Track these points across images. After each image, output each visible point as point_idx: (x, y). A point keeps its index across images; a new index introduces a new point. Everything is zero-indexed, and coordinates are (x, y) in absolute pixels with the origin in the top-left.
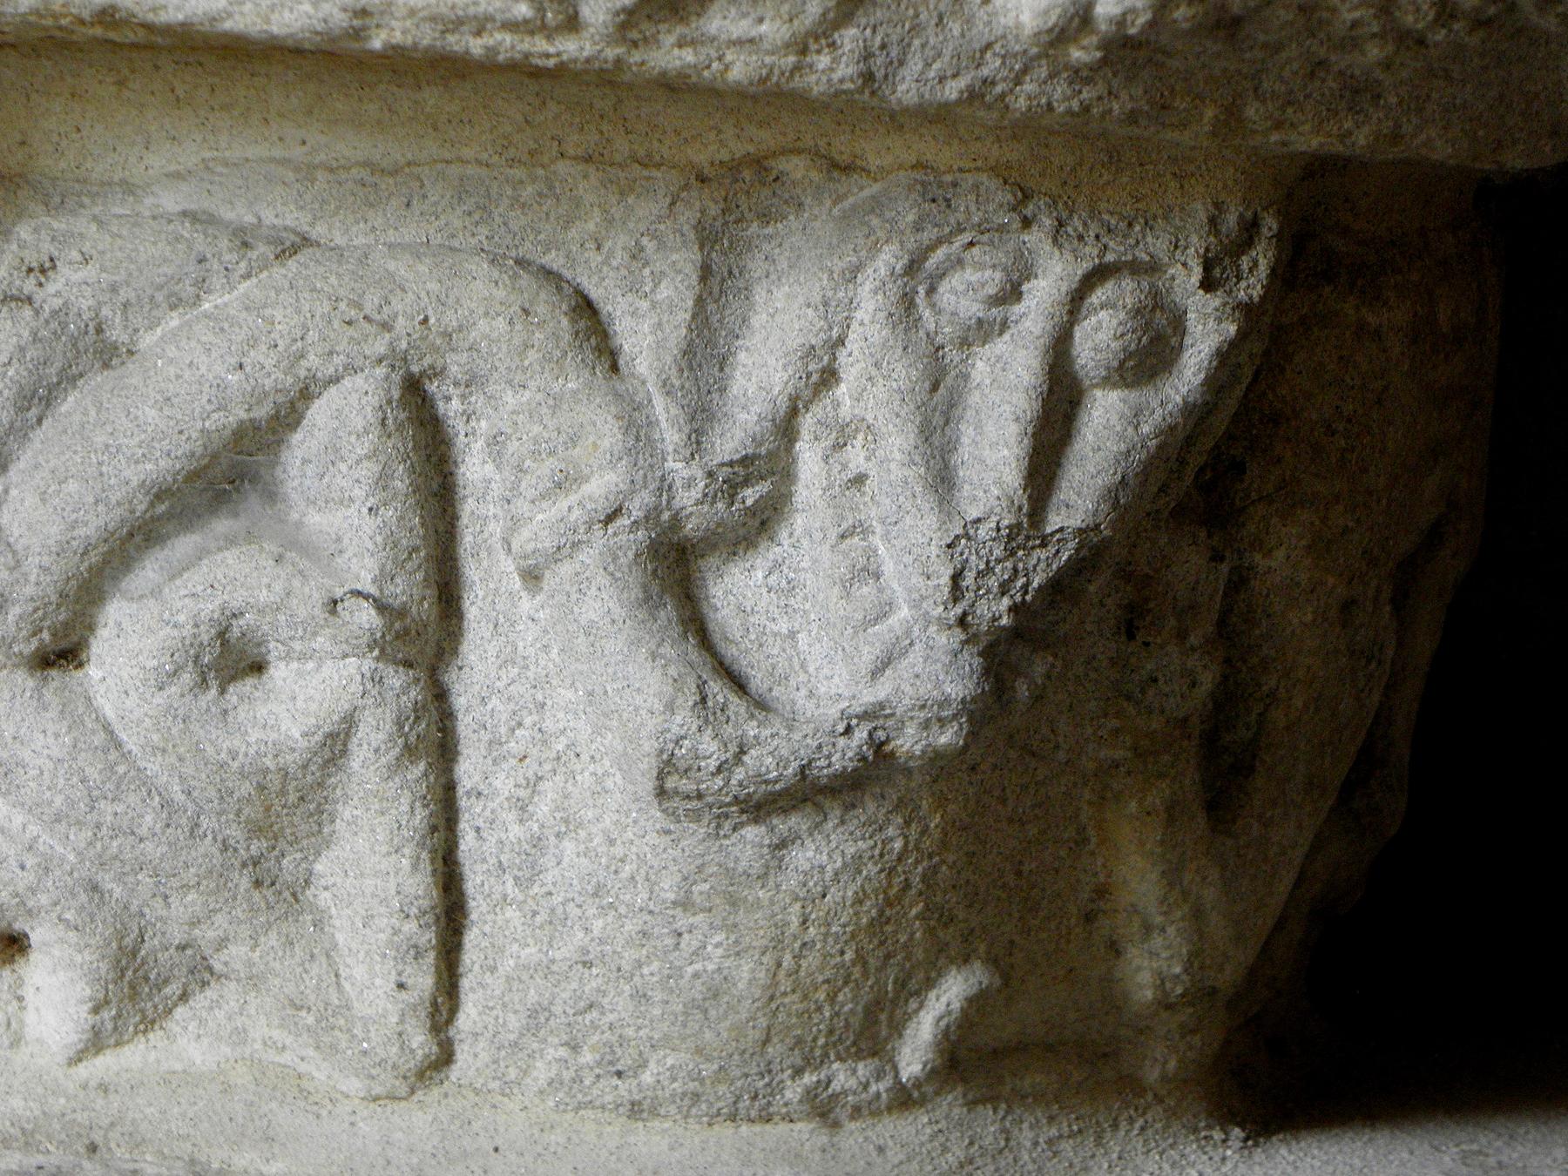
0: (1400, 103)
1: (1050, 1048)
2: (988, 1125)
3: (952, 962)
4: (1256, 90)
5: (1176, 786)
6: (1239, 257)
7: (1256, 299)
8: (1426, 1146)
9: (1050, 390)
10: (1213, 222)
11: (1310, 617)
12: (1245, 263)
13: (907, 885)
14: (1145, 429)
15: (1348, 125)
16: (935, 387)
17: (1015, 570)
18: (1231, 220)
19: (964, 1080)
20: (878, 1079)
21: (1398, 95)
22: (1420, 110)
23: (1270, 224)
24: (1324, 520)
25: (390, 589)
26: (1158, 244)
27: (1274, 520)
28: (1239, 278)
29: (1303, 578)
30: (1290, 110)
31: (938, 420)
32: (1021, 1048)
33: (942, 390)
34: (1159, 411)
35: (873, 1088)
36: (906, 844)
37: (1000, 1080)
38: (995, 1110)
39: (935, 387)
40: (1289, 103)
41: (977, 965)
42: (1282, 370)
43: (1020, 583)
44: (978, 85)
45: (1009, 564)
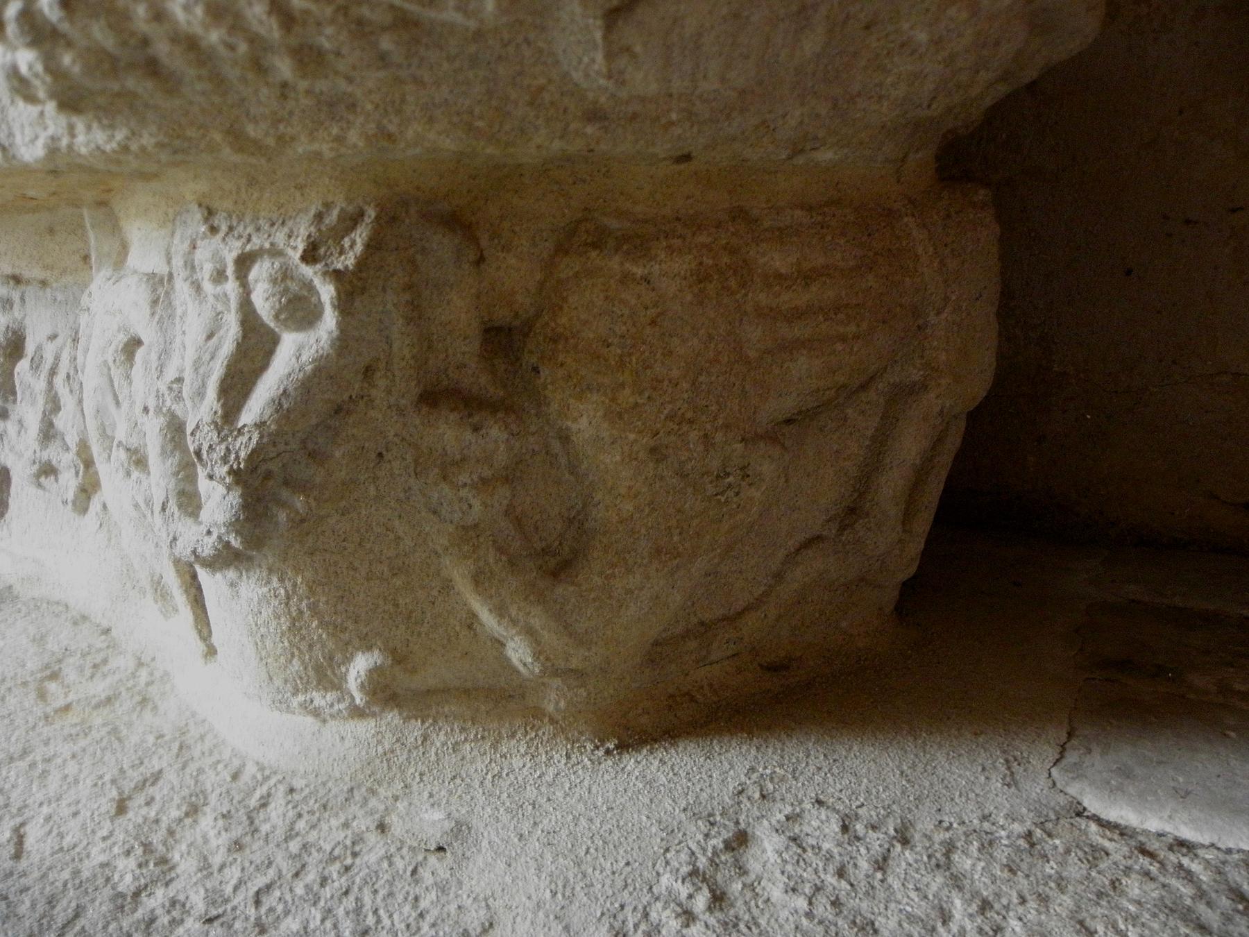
0: (377, 107)
1: (467, 692)
2: (415, 730)
3: (358, 649)
4: (248, 115)
5: (481, 564)
6: (343, 238)
7: (351, 267)
8: (795, 741)
9: (244, 337)
10: (319, 217)
11: (618, 458)
12: (346, 242)
13: (301, 612)
14: (304, 358)
15: (335, 131)
16: (210, 336)
17: (228, 449)
18: (332, 217)
19: (399, 706)
20: (339, 701)
21: (372, 102)
22: (399, 112)
23: (371, 213)
24: (613, 400)
25: (131, 440)
26: (280, 237)
27: (572, 401)
28: (341, 253)
29: (605, 434)
30: (281, 127)
31: (207, 357)
32: (445, 691)
33: (215, 339)
34: (315, 347)
35: (336, 707)
36: (286, 591)
37: (429, 707)
38: (423, 722)
39: (210, 336)
40: (280, 121)
41: (376, 652)
42: (561, 308)
43: (233, 456)
44: (49, 141)
45: (223, 446)
